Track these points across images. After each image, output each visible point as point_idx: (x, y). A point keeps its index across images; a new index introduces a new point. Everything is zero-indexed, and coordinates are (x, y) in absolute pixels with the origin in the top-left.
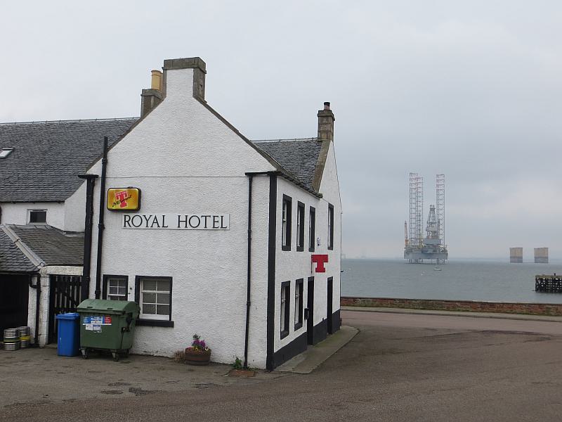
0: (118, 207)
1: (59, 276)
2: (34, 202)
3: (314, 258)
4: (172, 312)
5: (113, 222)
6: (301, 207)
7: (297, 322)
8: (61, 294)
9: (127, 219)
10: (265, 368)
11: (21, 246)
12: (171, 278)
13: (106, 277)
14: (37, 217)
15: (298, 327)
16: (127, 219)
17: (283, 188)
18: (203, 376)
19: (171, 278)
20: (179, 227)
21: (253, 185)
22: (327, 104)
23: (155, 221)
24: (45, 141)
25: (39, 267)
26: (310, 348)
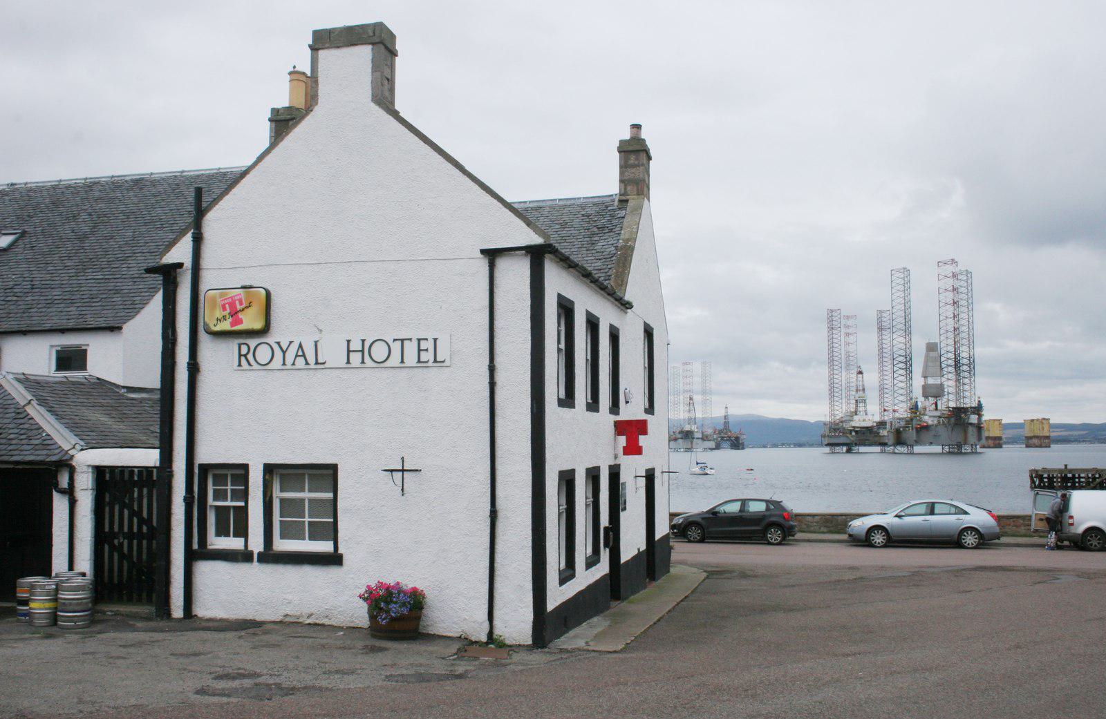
0: (226, 326)
1: (112, 469)
2: (63, 331)
3: (621, 428)
4: (340, 535)
5: (215, 356)
6: (593, 324)
7: (563, 565)
8: (117, 508)
9: (244, 350)
10: (530, 642)
11: (38, 413)
12: (334, 468)
13: (205, 469)
14: (70, 359)
15: (592, 562)
16: (244, 350)
17: (557, 282)
18: (406, 656)
19: (334, 468)
20: (348, 362)
21: (497, 274)
22: (637, 127)
23: (300, 353)
24: (84, 216)
25: (71, 452)
26: (616, 606)
